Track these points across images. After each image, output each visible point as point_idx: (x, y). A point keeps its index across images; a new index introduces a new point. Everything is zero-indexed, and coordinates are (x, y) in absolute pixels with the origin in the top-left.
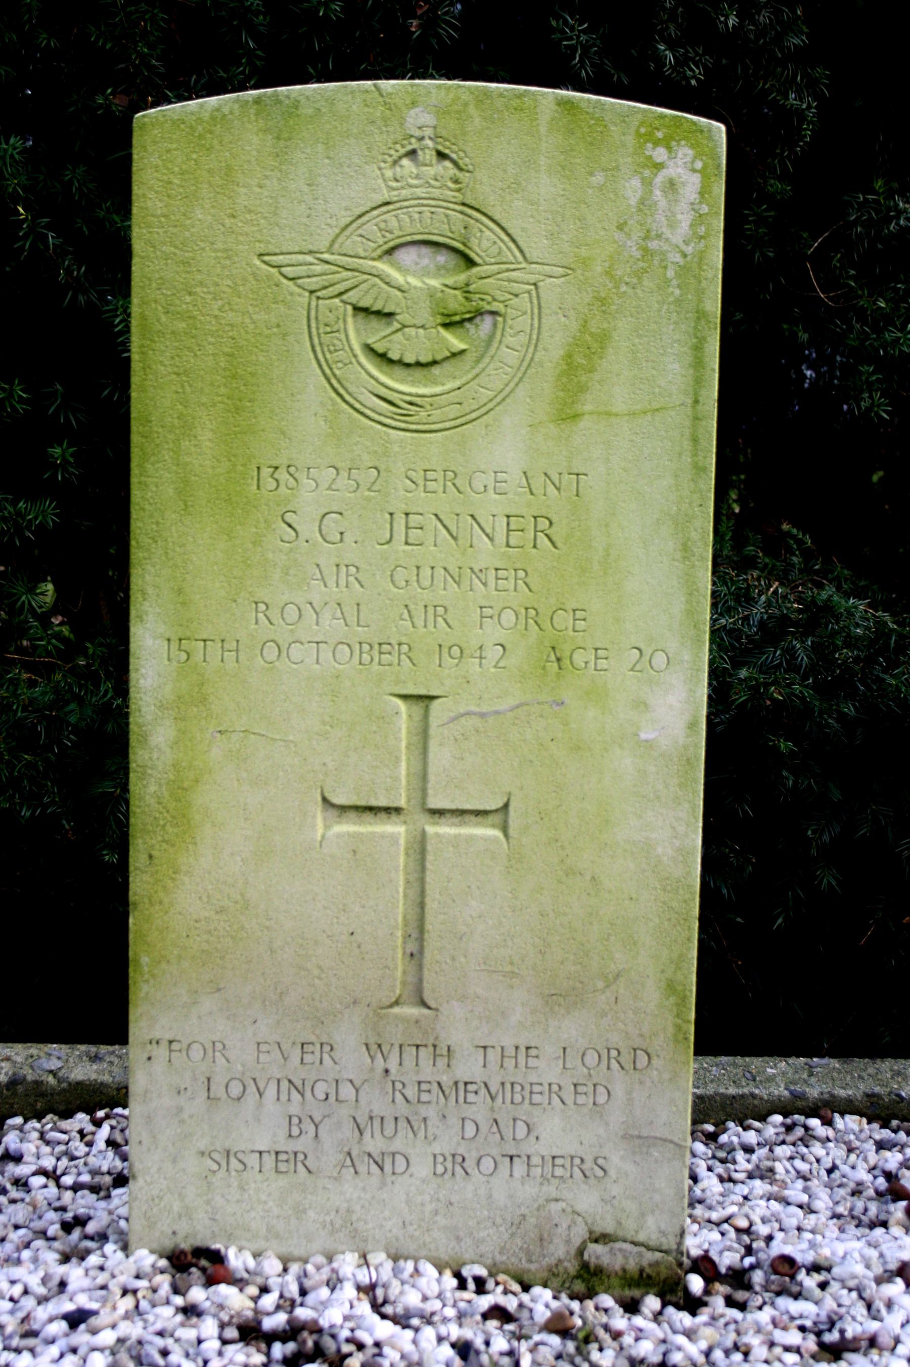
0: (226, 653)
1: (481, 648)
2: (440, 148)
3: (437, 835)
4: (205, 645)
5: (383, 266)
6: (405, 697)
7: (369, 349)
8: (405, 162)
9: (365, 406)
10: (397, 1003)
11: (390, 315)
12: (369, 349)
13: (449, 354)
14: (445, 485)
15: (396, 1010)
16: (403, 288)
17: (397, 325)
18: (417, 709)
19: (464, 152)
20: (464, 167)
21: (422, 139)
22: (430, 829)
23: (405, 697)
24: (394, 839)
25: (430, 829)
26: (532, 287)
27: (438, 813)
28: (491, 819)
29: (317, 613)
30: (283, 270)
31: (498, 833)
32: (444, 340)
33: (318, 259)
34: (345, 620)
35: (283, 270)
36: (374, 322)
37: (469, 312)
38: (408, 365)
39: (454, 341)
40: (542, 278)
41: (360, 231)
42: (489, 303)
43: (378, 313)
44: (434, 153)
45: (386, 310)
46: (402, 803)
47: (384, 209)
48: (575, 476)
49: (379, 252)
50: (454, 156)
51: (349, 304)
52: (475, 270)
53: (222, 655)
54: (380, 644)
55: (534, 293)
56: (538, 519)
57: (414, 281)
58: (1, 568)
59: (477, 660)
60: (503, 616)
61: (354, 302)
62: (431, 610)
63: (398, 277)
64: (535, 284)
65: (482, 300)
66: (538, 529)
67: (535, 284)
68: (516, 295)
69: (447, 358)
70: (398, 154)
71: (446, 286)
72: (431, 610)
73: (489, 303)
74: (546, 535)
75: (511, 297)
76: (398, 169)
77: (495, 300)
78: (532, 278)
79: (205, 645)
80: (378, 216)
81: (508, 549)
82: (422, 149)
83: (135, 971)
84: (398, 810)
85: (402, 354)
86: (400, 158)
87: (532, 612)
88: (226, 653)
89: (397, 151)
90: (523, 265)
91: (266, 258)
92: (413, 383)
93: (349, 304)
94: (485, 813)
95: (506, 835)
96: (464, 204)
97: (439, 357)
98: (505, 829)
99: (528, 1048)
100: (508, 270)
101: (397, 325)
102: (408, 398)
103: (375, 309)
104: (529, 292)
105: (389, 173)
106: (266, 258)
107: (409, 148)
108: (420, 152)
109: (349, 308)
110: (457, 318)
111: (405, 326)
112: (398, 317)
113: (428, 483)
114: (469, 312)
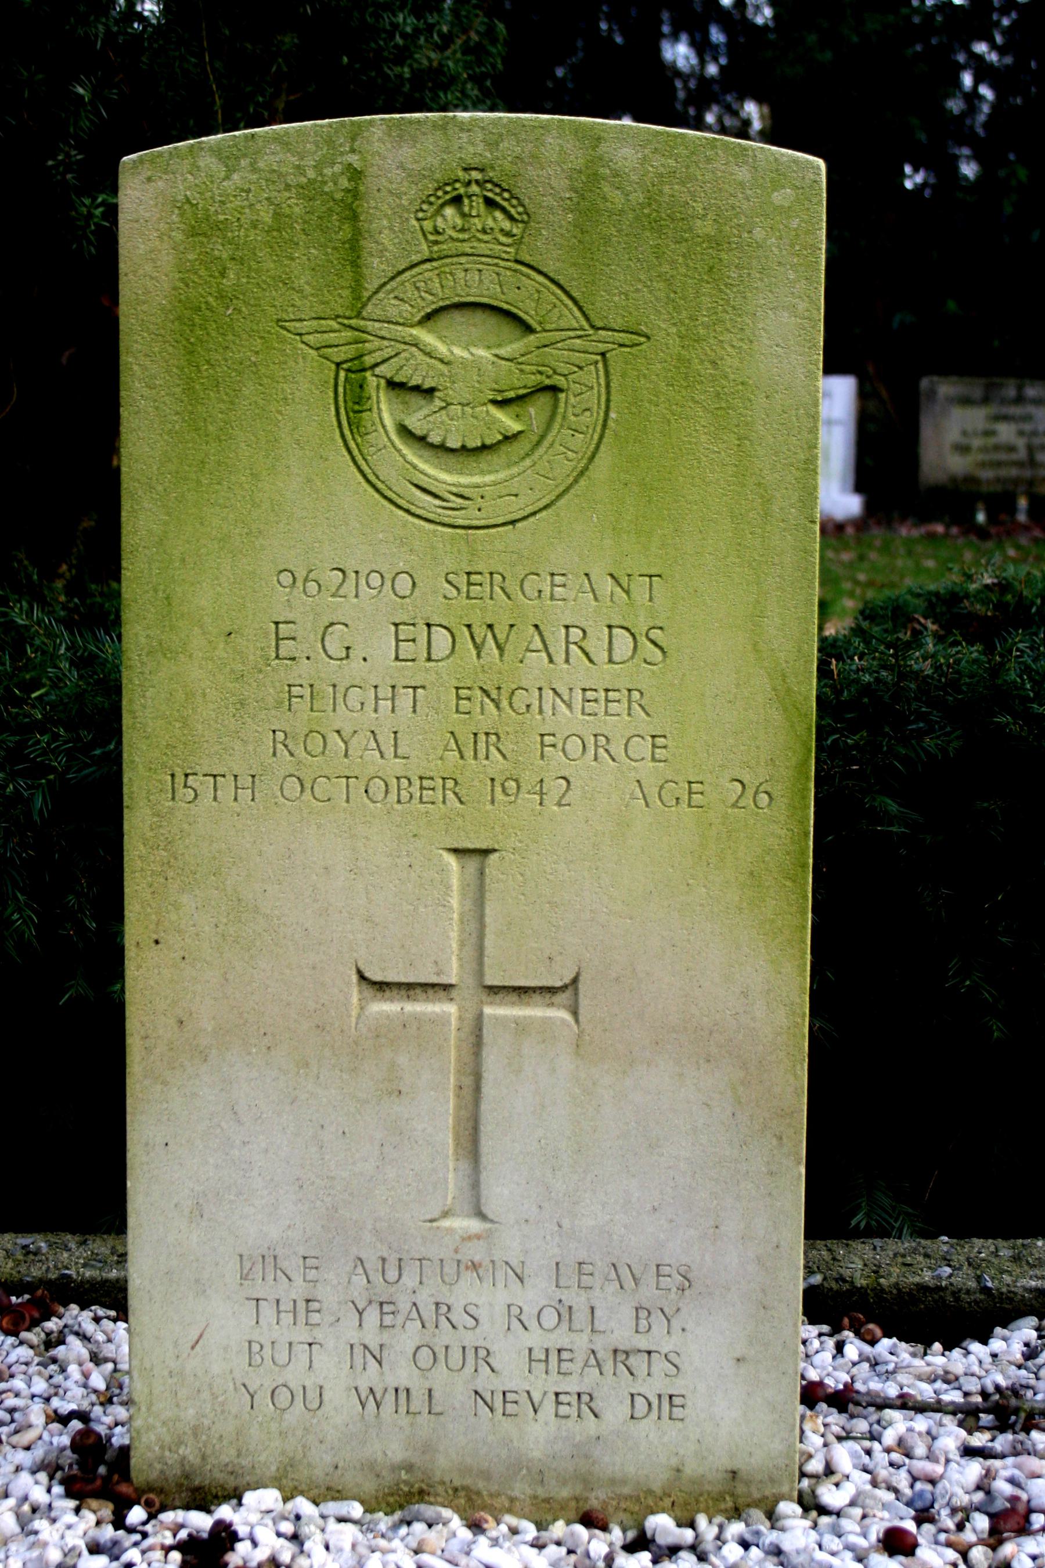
0: (240, 791)
1: (542, 781)
2: (490, 195)
3: (496, 1018)
4: (215, 782)
5: (426, 336)
6: (455, 851)
7: (404, 431)
8: (449, 211)
9: (377, 477)
10: (445, 1214)
11: (431, 391)
12: (404, 431)
13: (500, 437)
14: (629, 708)
15: (446, 1223)
16: (446, 360)
17: (438, 403)
18: (472, 864)
19: (517, 198)
20: (516, 216)
21: (468, 184)
22: (488, 1010)
23: (455, 851)
24: (442, 1020)
25: (488, 1010)
26: (599, 358)
27: (494, 990)
28: (562, 998)
29: (346, 743)
30: (306, 338)
31: (566, 1016)
32: (495, 421)
33: (344, 325)
34: (381, 752)
35: (306, 338)
36: (416, 400)
37: (525, 387)
38: (452, 450)
39: (507, 421)
40: (611, 346)
41: (396, 293)
42: (548, 377)
43: (417, 389)
44: (481, 200)
45: (426, 386)
46: (453, 981)
47: (428, 266)
48: (647, 579)
49: (418, 318)
50: (505, 204)
51: (382, 377)
52: (532, 337)
53: (236, 793)
54: (421, 778)
55: (600, 365)
56: (281, 626)
57: (458, 351)
58: (149, 7)
59: (537, 797)
60: (568, 747)
61: (389, 376)
62: (482, 738)
63: (442, 349)
64: (603, 354)
65: (540, 373)
66: (571, 640)
67: (603, 354)
68: (581, 368)
69: (499, 442)
70: (440, 202)
71: (496, 356)
72: (482, 738)
73: (548, 377)
74: (580, 648)
75: (576, 369)
76: (439, 220)
77: (555, 372)
78: (602, 347)
79: (215, 782)
80: (540, 284)
81: (399, 663)
82: (469, 197)
83: (132, 1122)
84: (447, 987)
85: (445, 438)
86: (443, 206)
87: (602, 740)
88: (240, 791)
89: (439, 198)
90: (591, 332)
91: (280, 324)
92: (449, 471)
93: (382, 377)
94: (551, 990)
95: (577, 1021)
96: (517, 261)
97: (488, 442)
98: (575, 1013)
99: (671, 1397)
100: (571, 338)
101: (438, 403)
102: (454, 490)
103: (413, 383)
104: (596, 362)
105: (428, 225)
106: (280, 324)
107: (455, 193)
108: (466, 201)
109: (383, 382)
110: (511, 394)
111: (448, 404)
112: (437, 394)
113: (556, 589)
114: (525, 387)
